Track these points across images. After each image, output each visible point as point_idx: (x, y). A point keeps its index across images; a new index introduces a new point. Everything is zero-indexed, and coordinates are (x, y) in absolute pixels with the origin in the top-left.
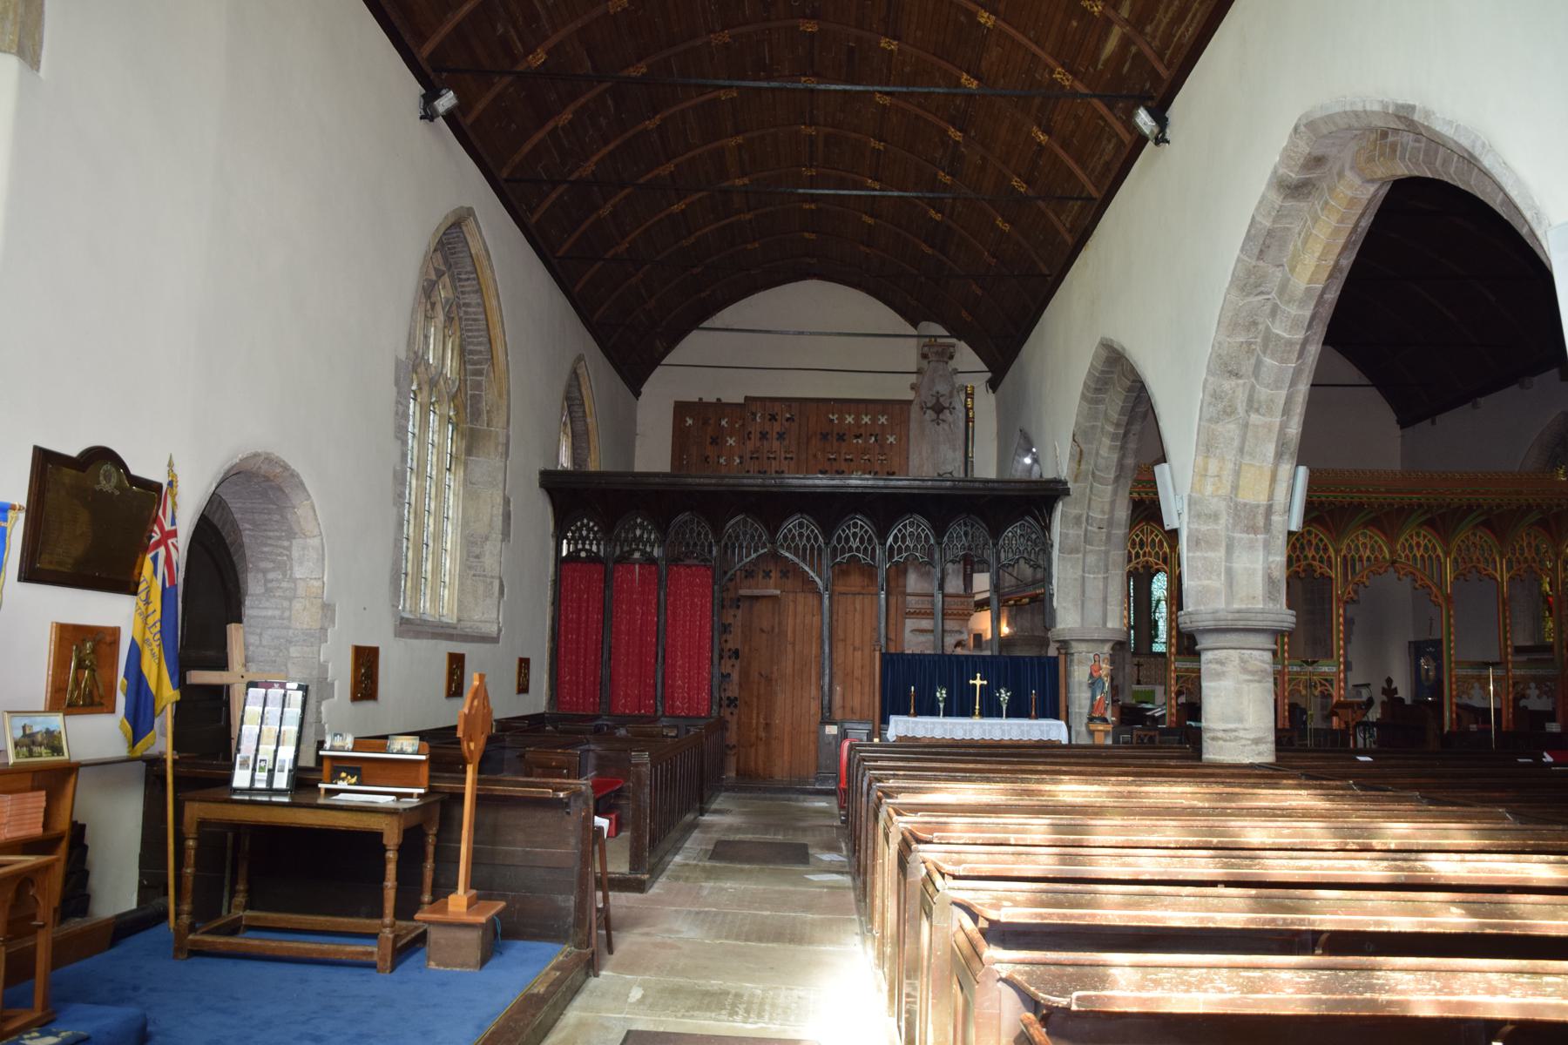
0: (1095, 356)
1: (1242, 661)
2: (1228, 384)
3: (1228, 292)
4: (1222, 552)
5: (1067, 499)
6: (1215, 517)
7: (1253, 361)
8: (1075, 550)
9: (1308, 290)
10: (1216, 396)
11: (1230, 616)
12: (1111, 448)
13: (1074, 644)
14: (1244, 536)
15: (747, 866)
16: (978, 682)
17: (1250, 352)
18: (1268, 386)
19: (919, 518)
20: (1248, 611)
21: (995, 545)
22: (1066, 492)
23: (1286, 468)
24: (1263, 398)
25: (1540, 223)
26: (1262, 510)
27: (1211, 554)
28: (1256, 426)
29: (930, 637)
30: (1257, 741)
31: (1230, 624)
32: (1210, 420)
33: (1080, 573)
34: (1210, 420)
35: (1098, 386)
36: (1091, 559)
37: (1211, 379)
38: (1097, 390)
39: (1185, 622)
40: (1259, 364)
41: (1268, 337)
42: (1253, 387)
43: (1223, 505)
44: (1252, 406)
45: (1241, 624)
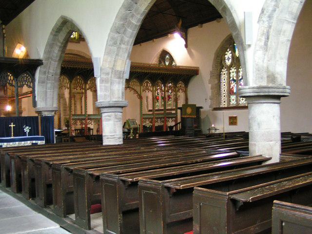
0: (58, 20)
1: (115, 116)
2: (116, 35)
3: (121, 9)
4: (109, 84)
5: (42, 66)
6: (108, 74)
7: (124, 30)
8: (43, 82)
9: (144, 11)
10: (113, 38)
11: (113, 103)
12: (59, 50)
13: (43, 112)
14: (117, 79)
15: (22, 182)
16: (12, 126)
17: (124, 27)
18: (128, 37)
19: (27, 74)
20: (118, 101)
21: (17, 80)
22: (42, 64)
23: (128, 60)
24: (126, 40)
25: (232, 9)
26: (122, 72)
27: (107, 85)
28: (123, 48)
29: (102, 112)
30: (119, 138)
31: (113, 105)
32: (110, 45)
33: (45, 90)
34: (110, 45)
35: (58, 30)
36: (49, 85)
37: (111, 33)
38: (57, 32)
39: (98, 104)
40: (125, 30)
41: (130, 23)
42: (123, 37)
43: (110, 71)
44: (122, 40)
45: (116, 105)
